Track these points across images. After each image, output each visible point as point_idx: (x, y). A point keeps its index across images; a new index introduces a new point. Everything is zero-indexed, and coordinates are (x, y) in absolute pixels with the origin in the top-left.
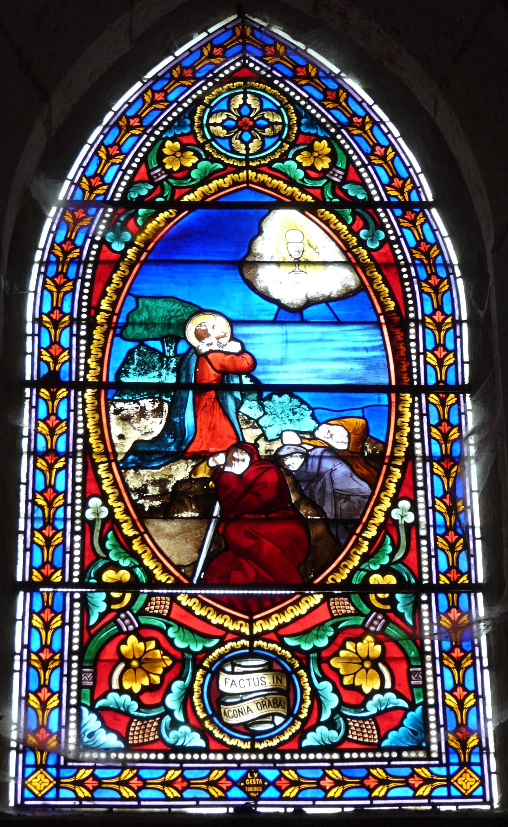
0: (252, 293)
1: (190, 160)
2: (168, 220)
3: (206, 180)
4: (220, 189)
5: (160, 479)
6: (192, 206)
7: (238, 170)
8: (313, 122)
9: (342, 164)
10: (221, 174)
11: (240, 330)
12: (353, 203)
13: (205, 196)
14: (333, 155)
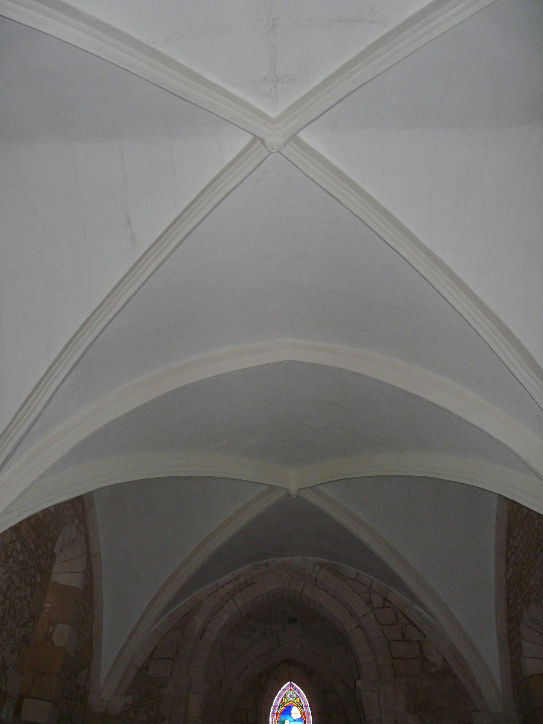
0: (259, 482)
1: (285, 701)
2: (283, 708)
3: (287, 703)
4: (288, 704)
5: (55, 554)
6: (286, 706)
7: (290, 702)
8: (297, 696)
9: (300, 701)
10: (288, 702)
11: (290, 722)
12: (301, 706)
13: (287, 705)
14: (299, 700)
